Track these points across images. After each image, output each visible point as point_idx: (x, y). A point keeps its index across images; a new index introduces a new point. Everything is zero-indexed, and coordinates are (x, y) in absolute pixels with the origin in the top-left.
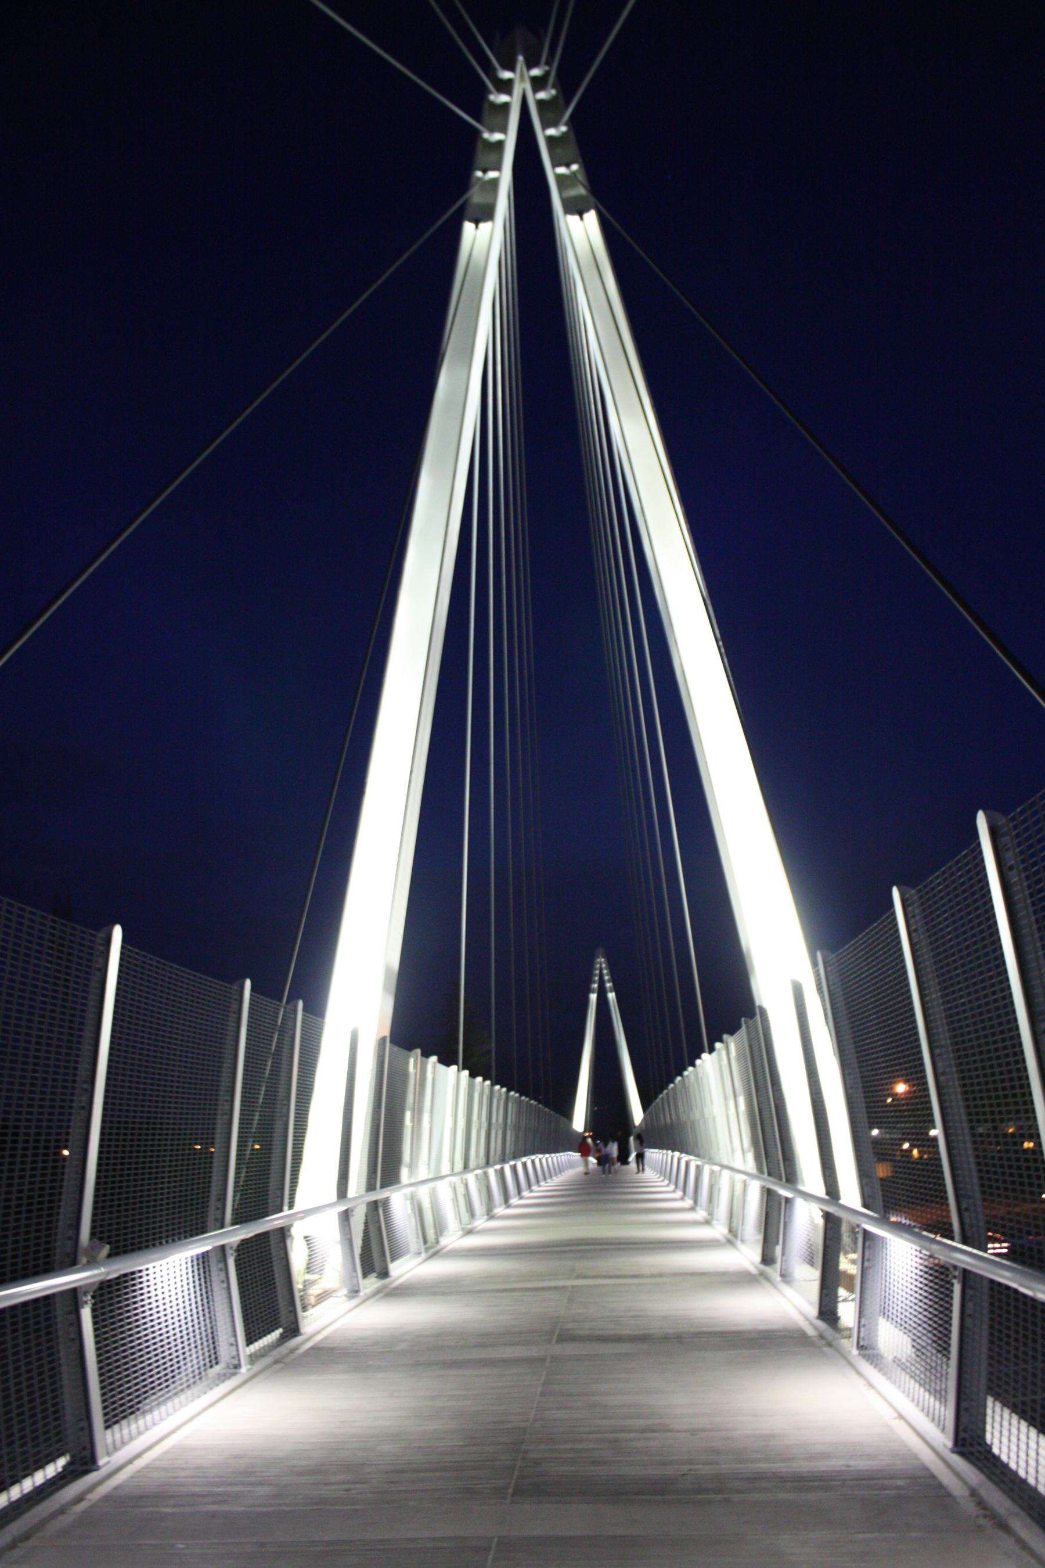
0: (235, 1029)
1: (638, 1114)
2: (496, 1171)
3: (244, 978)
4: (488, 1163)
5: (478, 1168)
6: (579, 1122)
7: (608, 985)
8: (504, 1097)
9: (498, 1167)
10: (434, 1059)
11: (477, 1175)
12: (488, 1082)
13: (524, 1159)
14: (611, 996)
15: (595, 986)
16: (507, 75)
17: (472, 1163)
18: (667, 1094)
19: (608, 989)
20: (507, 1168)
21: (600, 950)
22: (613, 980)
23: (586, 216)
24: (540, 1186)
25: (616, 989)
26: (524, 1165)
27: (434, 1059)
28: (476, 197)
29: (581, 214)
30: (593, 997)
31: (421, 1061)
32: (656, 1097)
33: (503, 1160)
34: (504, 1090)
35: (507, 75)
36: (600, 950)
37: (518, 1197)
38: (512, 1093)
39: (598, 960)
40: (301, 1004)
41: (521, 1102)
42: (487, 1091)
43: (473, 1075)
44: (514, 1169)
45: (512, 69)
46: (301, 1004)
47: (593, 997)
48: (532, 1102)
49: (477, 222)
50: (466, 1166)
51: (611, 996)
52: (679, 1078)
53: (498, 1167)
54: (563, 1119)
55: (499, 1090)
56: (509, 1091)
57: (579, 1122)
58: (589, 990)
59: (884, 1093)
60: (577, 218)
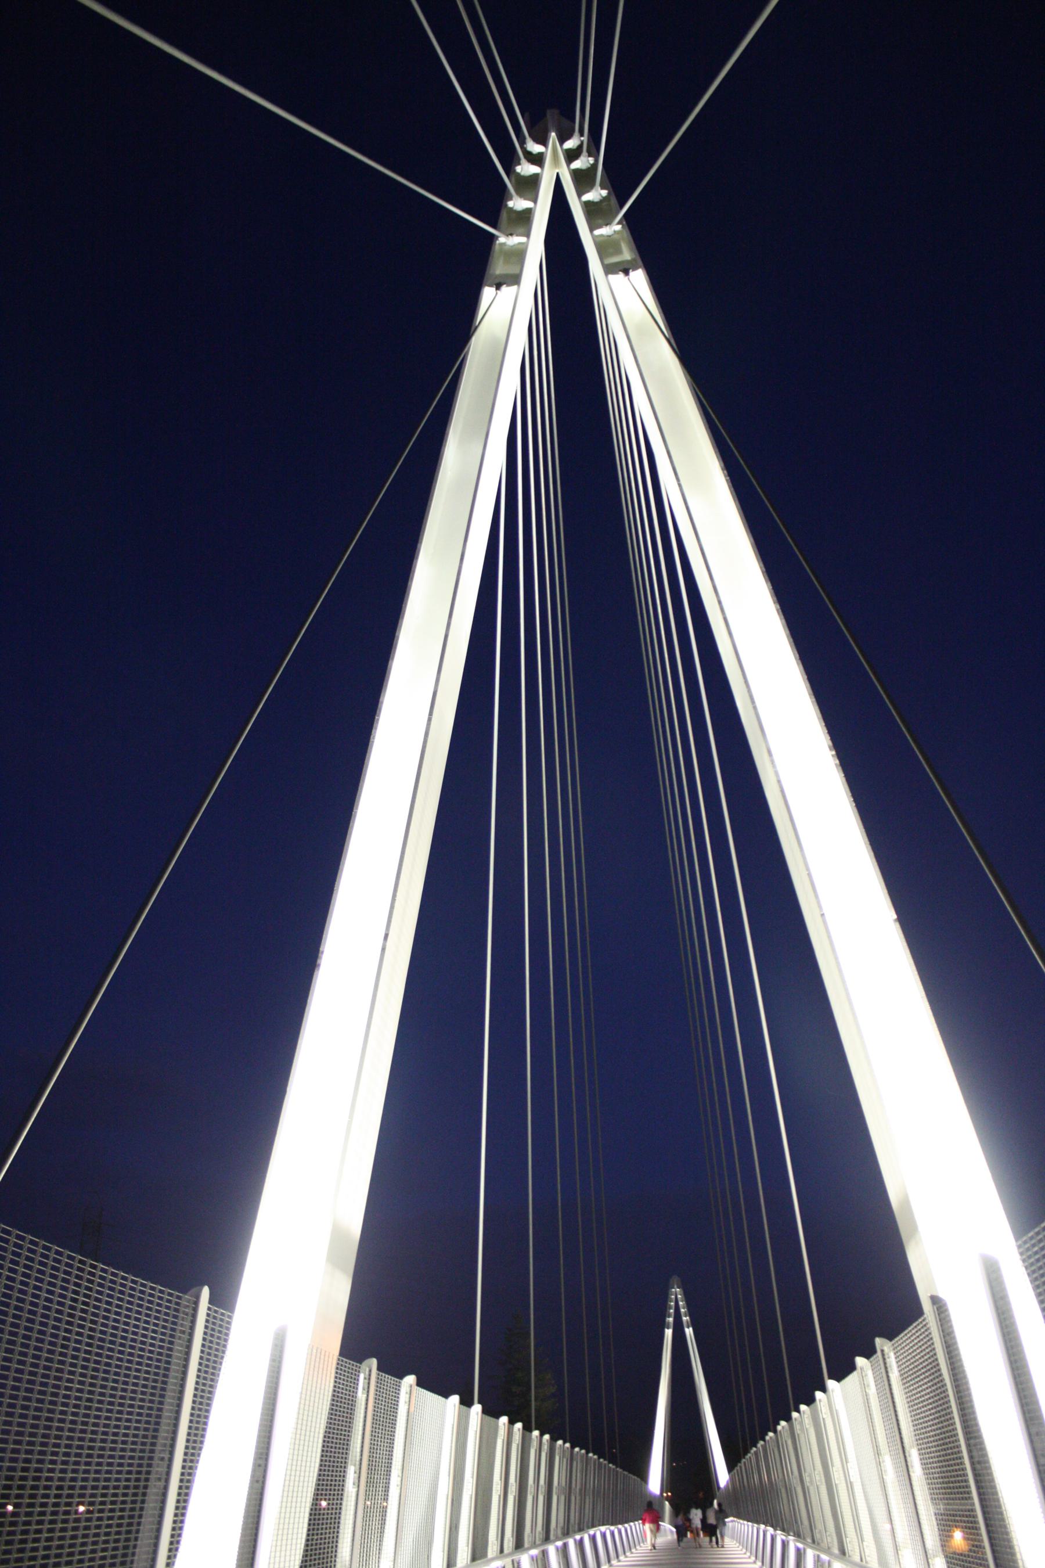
0: (183, 1356)
1: (723, 1476)
2: (557, 1548)
3: (202, 1285)
4: (547, 1539)
5: (534, 1545)
6: (655, 1483)
7: (685, 1319)
8: (568, 1454)
9: (559, 1543)
10: (410, 1379)
11: (532, 1558)
12: (568, 1445)
13: (592, 1532)
14: (689, 1332)
15: (671, 1320)
16: (536, 148)
17: (506, 1551)
18: (756, 1453)
19: (682, 1314)
20: (571, 1542)
21: (675, 1279)
22: (691, 1313)
23: (632, 274)
24: (619, 1561)
25: (694, 1324)
26: (593, 1539)
27: (410, 1379)
28: (498, 267)
29: (626, 272)
30: (669, 1333)
31: (379, 1381)
32: (746, 1451)
33: (567, 1533)
34: (568, 1445)
35: (536, 148)
36: (675, 1279)
37: (616, 1560)
38: (577, 1449)
39: (673, 1290)
40: (206, 1292)
41: (600, 1464)
42: (545, 1447)
43: (491, 1411)
44: (580, 1544)
45: (543, 142)
46: (206, 1292)
47: (669, 1333)
48: (611, 1465)
49: (498, 287)
50: (519, 1545)
51: (689, 1332)
52: (754, 1449)
53: (578, 1537)
54: (643, 1483)
55: (562, 1447)
56: (573, 1447)
57: (655, 1483)
58: (663, 1325)
59: (937, 1459)
60: (621, 275)
